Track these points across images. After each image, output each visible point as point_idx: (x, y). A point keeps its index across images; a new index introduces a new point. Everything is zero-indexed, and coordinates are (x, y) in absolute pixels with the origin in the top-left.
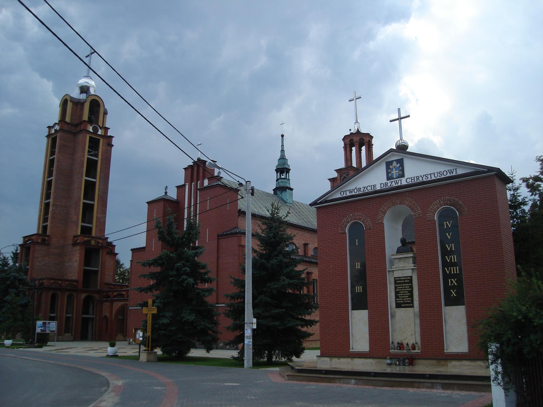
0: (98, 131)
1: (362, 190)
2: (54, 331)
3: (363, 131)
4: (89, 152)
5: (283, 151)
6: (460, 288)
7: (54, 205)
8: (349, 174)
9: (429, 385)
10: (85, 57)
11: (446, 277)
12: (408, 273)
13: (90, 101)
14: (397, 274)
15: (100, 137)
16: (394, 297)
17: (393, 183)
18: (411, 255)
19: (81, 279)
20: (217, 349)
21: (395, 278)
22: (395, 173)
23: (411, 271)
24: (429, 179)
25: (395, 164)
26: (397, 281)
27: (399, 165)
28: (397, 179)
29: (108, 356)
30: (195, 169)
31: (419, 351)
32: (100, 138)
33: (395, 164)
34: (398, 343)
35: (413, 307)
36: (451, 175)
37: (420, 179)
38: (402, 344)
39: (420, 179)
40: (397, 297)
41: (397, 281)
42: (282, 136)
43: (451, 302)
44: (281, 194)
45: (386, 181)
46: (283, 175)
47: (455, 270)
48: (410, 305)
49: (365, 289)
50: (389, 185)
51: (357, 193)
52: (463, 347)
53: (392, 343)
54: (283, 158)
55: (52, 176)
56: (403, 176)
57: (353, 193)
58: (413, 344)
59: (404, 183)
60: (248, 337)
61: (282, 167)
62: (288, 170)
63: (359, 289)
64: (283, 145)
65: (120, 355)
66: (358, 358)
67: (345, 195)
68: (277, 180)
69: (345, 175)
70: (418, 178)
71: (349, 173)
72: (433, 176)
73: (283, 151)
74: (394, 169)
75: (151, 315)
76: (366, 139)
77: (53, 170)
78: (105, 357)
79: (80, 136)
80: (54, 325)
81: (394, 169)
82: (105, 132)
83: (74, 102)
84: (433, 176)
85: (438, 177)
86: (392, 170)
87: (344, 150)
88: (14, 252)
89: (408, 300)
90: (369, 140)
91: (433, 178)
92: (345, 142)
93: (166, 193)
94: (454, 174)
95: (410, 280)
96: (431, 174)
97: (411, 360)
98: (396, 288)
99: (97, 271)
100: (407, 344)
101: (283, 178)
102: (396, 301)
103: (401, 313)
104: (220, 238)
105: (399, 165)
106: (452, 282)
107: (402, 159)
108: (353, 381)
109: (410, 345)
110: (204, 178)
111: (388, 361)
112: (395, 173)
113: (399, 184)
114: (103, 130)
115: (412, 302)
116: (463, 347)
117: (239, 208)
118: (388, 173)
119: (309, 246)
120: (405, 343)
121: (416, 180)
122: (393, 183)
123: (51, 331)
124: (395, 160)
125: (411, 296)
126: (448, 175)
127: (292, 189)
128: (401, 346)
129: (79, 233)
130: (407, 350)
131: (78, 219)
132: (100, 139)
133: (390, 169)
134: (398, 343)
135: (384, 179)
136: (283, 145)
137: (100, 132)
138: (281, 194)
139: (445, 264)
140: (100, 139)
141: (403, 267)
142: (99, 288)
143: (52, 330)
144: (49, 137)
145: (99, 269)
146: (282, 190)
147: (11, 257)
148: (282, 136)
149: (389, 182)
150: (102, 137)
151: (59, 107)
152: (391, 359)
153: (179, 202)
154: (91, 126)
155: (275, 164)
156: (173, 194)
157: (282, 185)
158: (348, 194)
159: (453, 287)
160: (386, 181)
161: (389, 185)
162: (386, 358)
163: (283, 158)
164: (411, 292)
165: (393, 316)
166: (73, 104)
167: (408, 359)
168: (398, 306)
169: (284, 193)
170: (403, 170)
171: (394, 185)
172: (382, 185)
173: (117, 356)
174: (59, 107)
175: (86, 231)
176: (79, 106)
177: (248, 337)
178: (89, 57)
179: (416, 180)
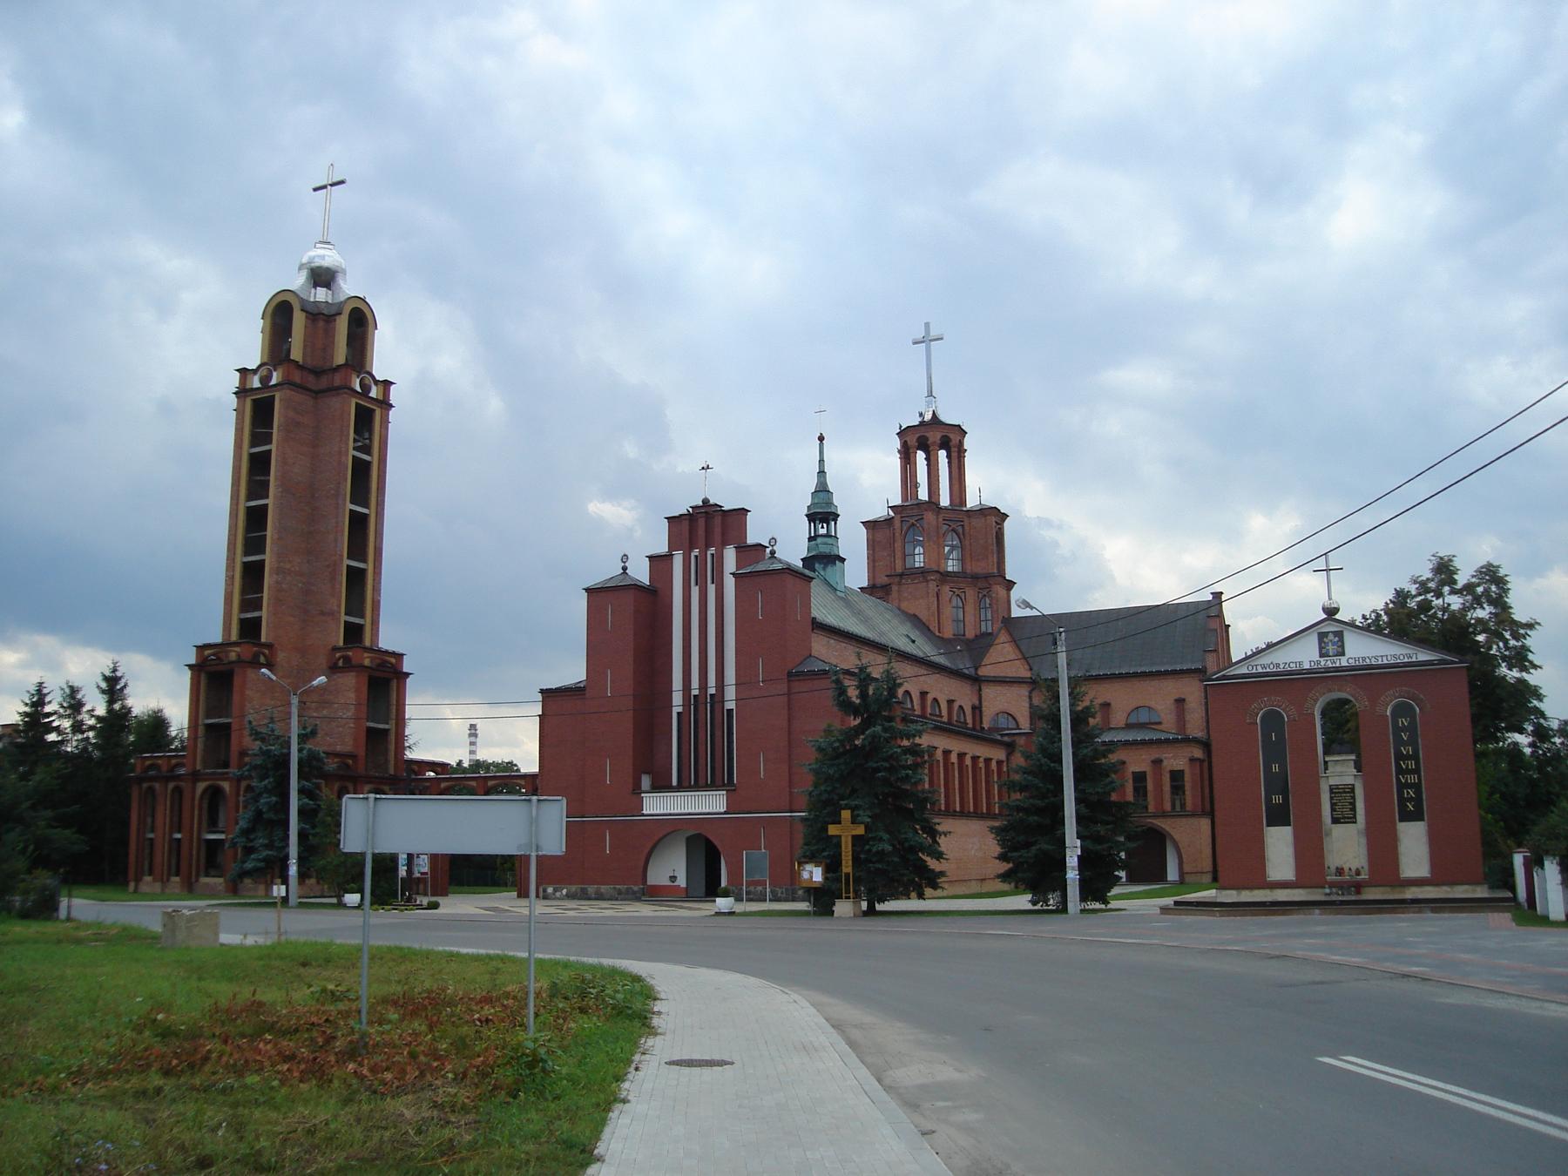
0: (369, 391)
1: (1282, 666)
2: (426, 873)
3: (947, 417)
4: (355, 441)
5: (822, 473)
6: (1418, 801)
7: (278, 571)
8: (922, 519)
9: (1417, 909)
10: (312, 191)
11: (1401, 787)
12: (1349, 780)
13: (349, 311)
14: (1332, 781)
15: (375, 405)
16: (1330, 811)
17: (1329, 662)
18: (1354, 758)
19: (362, 752)
20: (793, 901)
21: (1330, 786)
22: (1331, 649)
23: (1353, 777)
24: (1380, 662)
25: (1331, 637)
26: (1333, 790)
27: (1337, 639)
28: (1334, 658)
29: (718, 914)
30: (701, 522)
31: (1367, 877)
32: (374, 408)
33: (1331, 637)
34: (1337, 868)
35: (1355, 822)
36: (1410, 660)
37: (1368, 660)
38: (1342, 869)
39: (1368, 660)
40: (1333, 810)
41: (1333, 790)
42: (821, 439)
43: (1407, 817)
44: (824, 569)
45: (1318, 659)
46: (823, 527)
47: (1412, 779)
48: (1352, 820)
49: (1286, 799)
50: (1323, 663)
51: (1275, 670)
52: (1423, 871)
53: (1329, 868)
54: (822, 490)
55: (267, 497)
56: (1343, 654)
57: (1268, 670)
58: (1357, 869)
59: (1344, 663)
60: (1073, 868)
61: (826, 511)
62: (835, 516)
63: (1277, 799)
64: (821, 461)
65: (737, 911)
66: (1282, 888)
67: (1254, 671)
68: (811, 539)
69: (912, 521)
70: (1364, 659)
71: (924, 516)
72: (1384, 658)
73: (822, 473)
74: (1330, 644)
75: (850, 839)
76: (954, 438)
77: (269, 481)
78: (714, 915)
79: (335, 402)
80: (426, 861)
81: (1330, 644)
82: (384, 390)
83: (311, 313)
84: (1384, 658)
85: (1392, 662)
86: (1327, 644)
87: (900, 458)
88: (108, 673)
89: (1349, 814)
90: (960, 441)
91: (1385, 662)
92: (906, 441)
93: (625, 569)
94: (1414, 659)
95: (1352, 789)
96: (1382, 656)
97: (1358, 887)
98: (1331, 798)
99: (386, 732)
100: (1350, 869)
101: (822, 536)
102: (1332, 815)
103: (1339, 831)
104: (792, 679)
105: (1337, 639)
106: (1408, 793)
107: (1342, 632)
108: (1317, 911)
109: (1354, 869)
110: (725, 543)
111: (1327, 891)
112: (1331, 649)
113: (1338, 665)
114: (381, 387)
115: (1355, 817)
116: (1423, 871)
117: (813, 616)
118: (1321, 648)
119: (929, 695)
120: (1346, 868)
121: (1361, 661)
122: (1329, 662)
123: (422, 874)
124: (1332, 632)
125: (1354, 809)
126: (1406, 660)
127: (843, 560)
128: (1340, 871)
129: (341, 643)
130: (1349, 876)
131: (339, 606)
132: (374, 410)
133: (1325, 643)
134: (1337, 868)
135: (1316, 657)
136: (821, 461)
137: (373, 394)
138: (824, 569)
139: (1400, 771)
140: (374, 410)
141: (1342, 772)
142: (392, 771)
143: (422, 871)
144: (245, 397)
145: (391, 726)
146: (825, 561)
147: (98, 687)
148: (821, 439)
149: (1322, 659)
150: (379, 405)
151: (262, 318)
152: (1330, 887)
153: (656, 591)
154: (358, 377)
155: (803, 501)
156: (641, 573)
157: (824, 549)
158: (1260, 670)
159: (1410, 799)
160: (1318, 659)
161: (1323, 663)
162: (1324, 887)
163: (822, 490)
164: (1353, 804)
165: (1329, 834)
166: (307, 317)
167: (1354, 887)
168: (1335, 821)
169: (830, 569)
170: (1343, 646)
171: (1331, 665)
172: (1313, 664)
173: (734, 912)
174: (262, 318)
175: (354, 633)
176: (321, 324)
177: (1073, 868)
178: (325, 190)
179: (1361, 661)
